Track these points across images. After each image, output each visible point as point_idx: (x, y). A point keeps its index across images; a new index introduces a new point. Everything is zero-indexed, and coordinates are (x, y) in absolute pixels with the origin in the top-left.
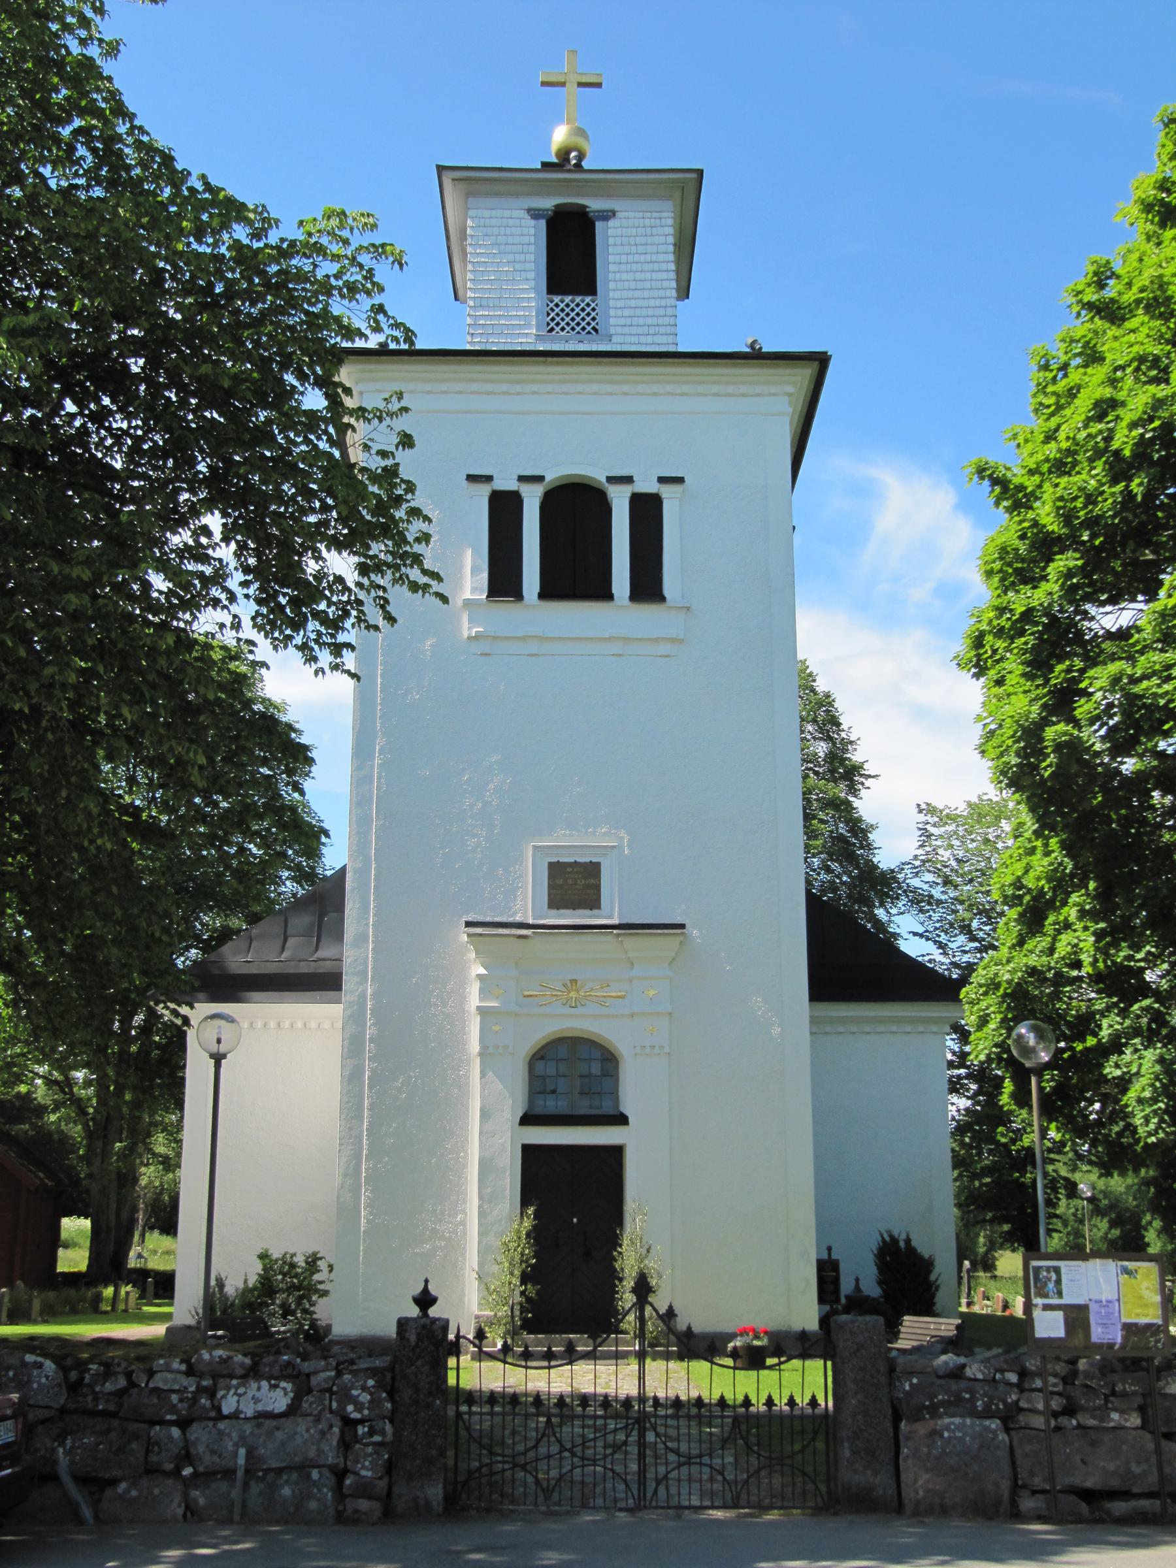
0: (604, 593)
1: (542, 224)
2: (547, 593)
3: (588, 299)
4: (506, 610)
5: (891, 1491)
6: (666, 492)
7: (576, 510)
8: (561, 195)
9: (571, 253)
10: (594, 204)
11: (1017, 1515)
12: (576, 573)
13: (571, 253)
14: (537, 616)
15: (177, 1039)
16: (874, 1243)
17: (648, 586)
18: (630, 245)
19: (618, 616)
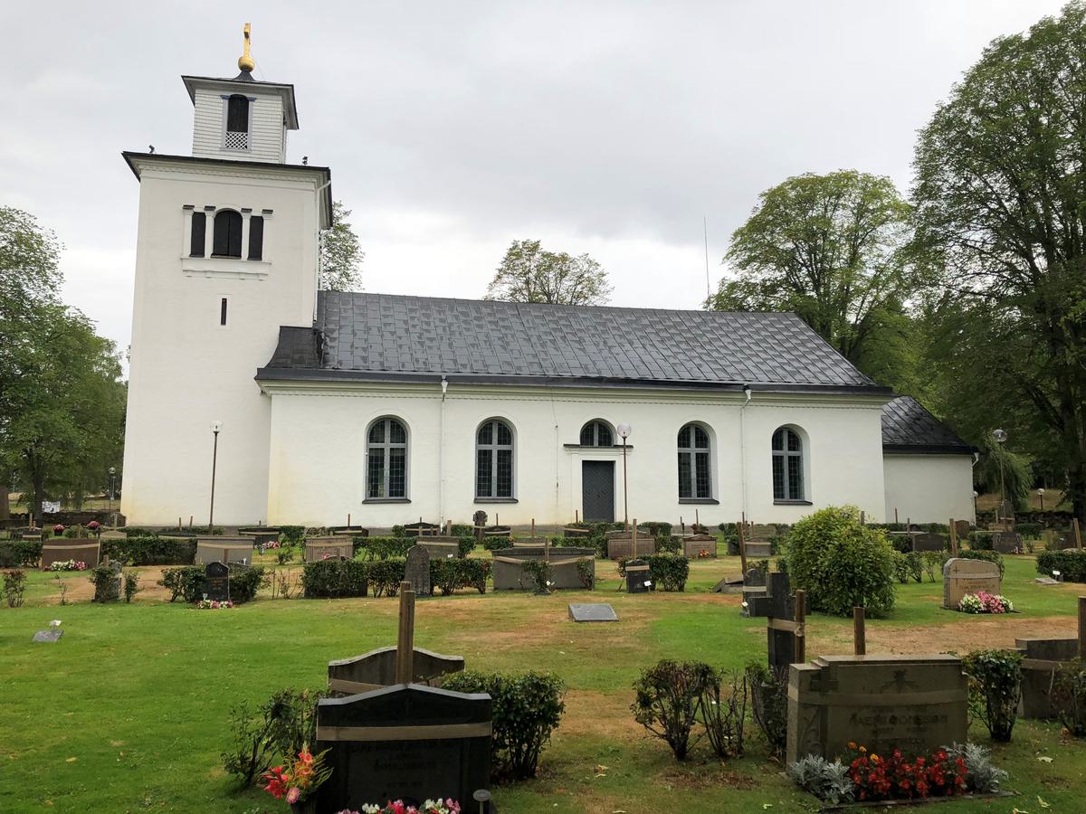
0: (238, 255)
1: (227, 101)
2: (215, 254)
3: (245, 134)
4: (197, 264)
5: (1043, 501)
6: (265, 217)
7: (229, 219)
8: (234, 91)
9: (238, 118)
10: (248, 95)
11: (687, 736)
12: (227, 247)
13: (238, 118)
14: (208, 263)
15: (415, 652)
16: (251, 64)
17: (256, 254)
18: (263, 113)
19: (243, 265)
